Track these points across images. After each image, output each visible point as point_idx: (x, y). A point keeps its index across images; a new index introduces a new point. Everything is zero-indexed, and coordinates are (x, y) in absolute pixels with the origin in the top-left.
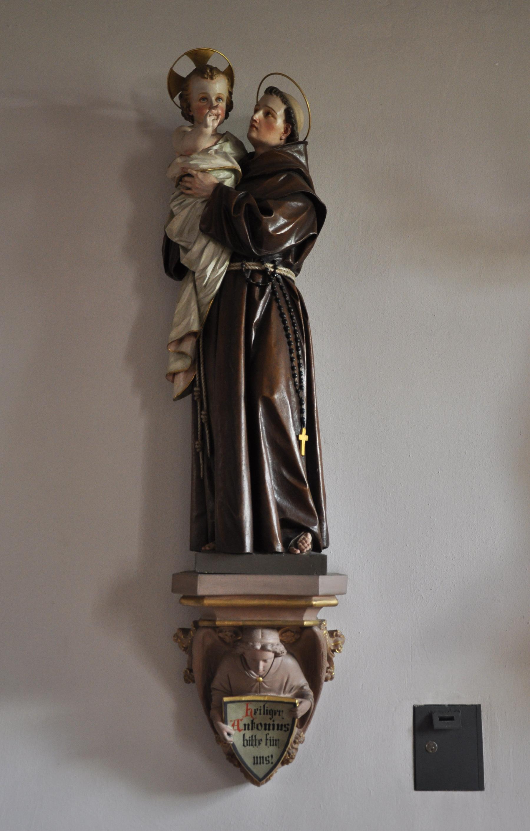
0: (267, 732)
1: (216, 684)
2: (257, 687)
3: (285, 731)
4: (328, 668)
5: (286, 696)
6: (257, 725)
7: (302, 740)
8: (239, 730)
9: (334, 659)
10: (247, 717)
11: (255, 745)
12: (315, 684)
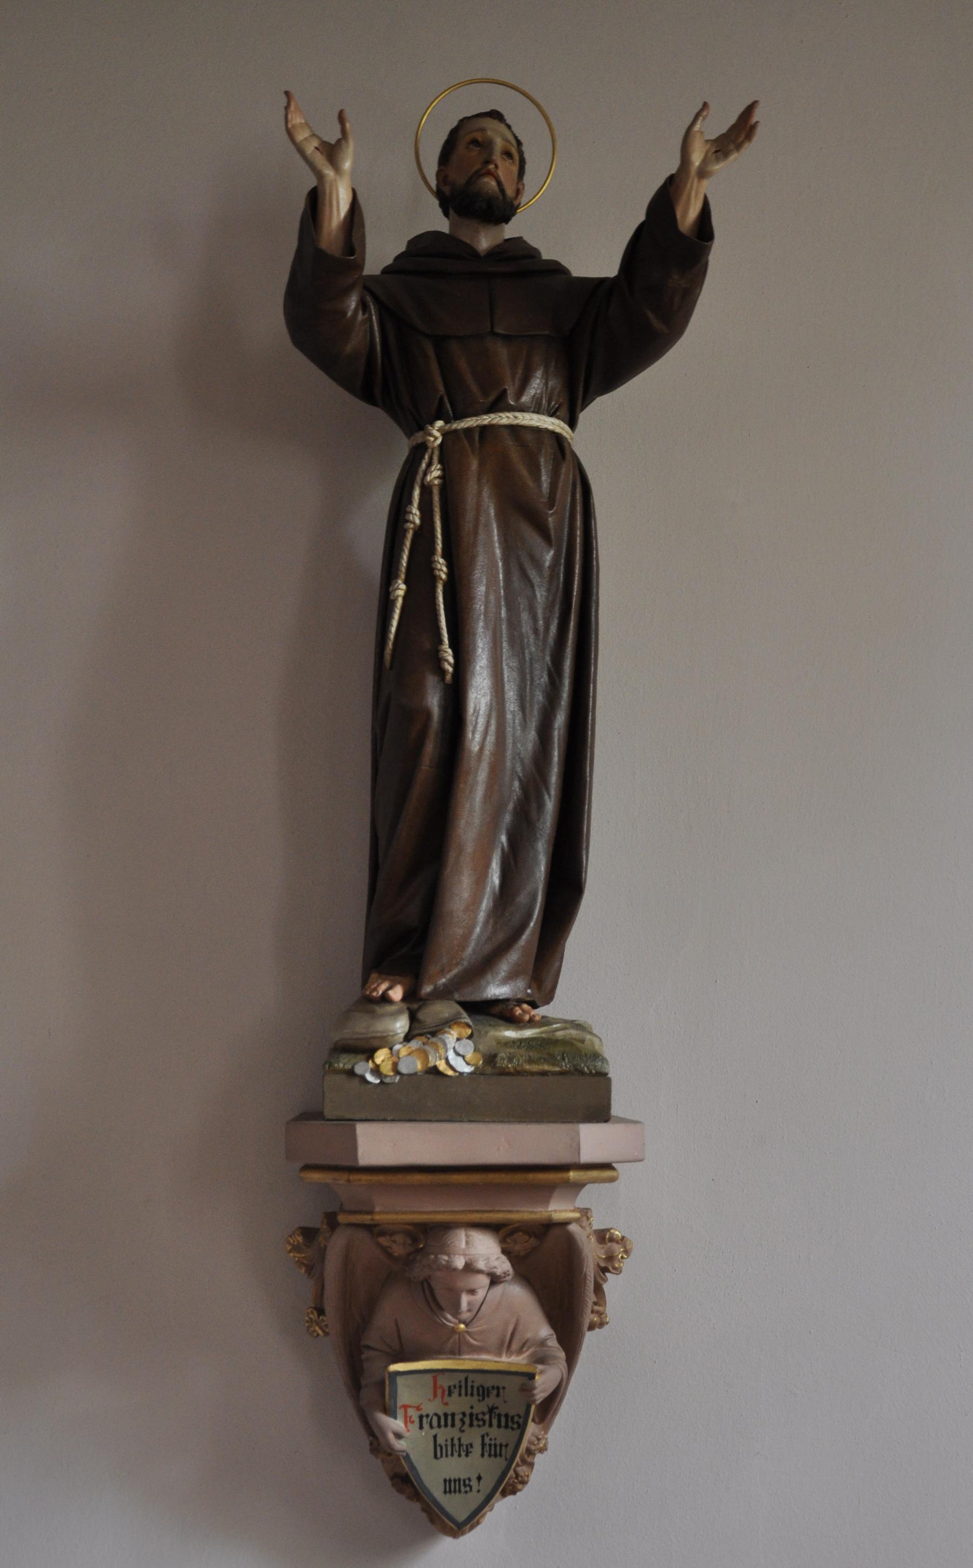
1: (372, 1338)
4: (595, 1304)
5: (507, 1361)
9: (606, 1287)
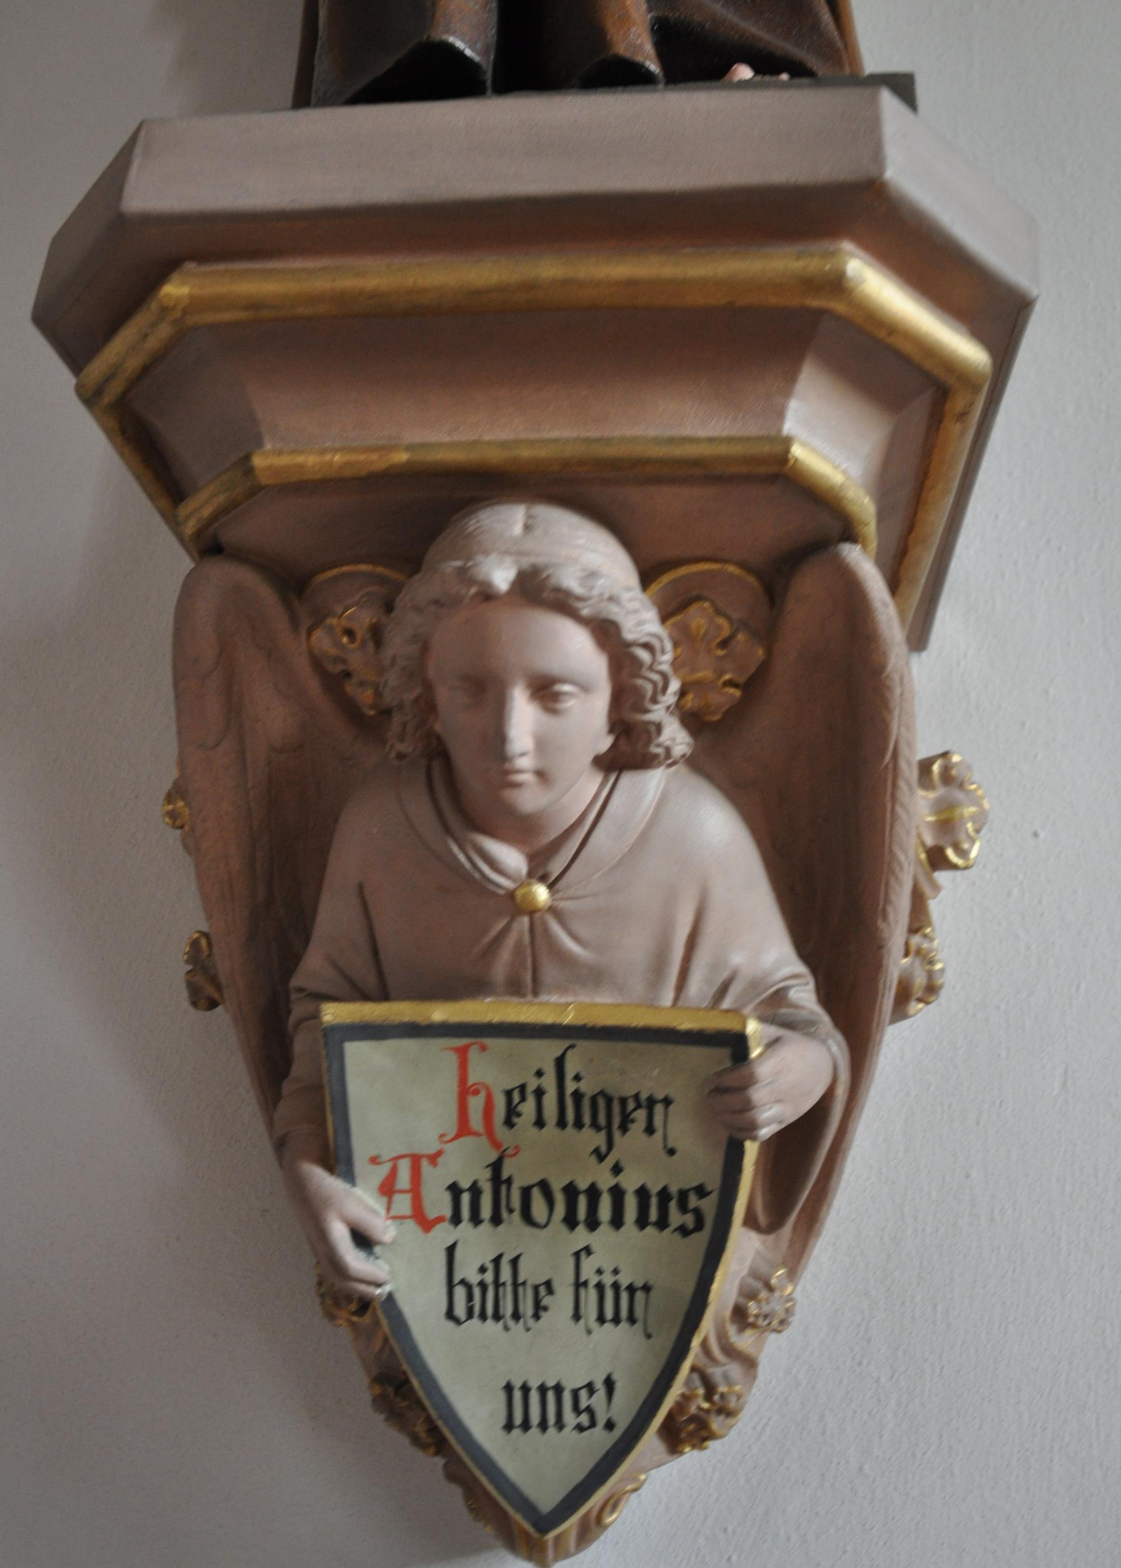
0: (581, 1237)
1: (314, 966)
2: (518, 949)
3: (684, 1231)
6: (526, 1193)
7: (776, 1305)
8: (427, 1225)
9: (935, 907)
10: (467, 1140)
11: (516, 1316)
12: (850, 961)
